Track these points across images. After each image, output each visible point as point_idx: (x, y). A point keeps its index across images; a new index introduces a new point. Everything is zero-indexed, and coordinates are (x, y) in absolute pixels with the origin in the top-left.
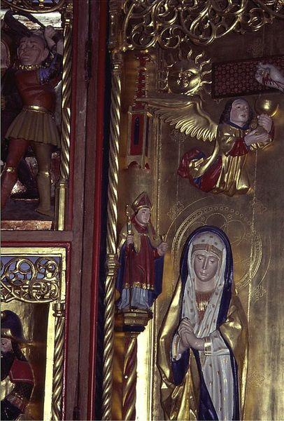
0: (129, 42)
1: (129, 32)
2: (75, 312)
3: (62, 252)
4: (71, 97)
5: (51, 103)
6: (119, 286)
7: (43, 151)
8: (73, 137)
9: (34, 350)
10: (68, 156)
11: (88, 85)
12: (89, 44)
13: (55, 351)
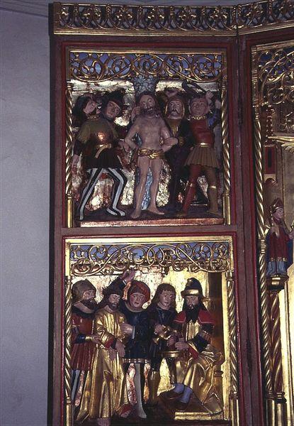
0: (266, 100)
1: (265, 93)
2: (242, 277)
3: (230, 238)
4: (228, 109)
5: (211, 139)
6: (267, 259)
7: (211, 173)
8: (232, 170)
9: (212, 304)
10: (229, 182)
11: (241, 128)
12: (240, 102)
13: (228, 294)
